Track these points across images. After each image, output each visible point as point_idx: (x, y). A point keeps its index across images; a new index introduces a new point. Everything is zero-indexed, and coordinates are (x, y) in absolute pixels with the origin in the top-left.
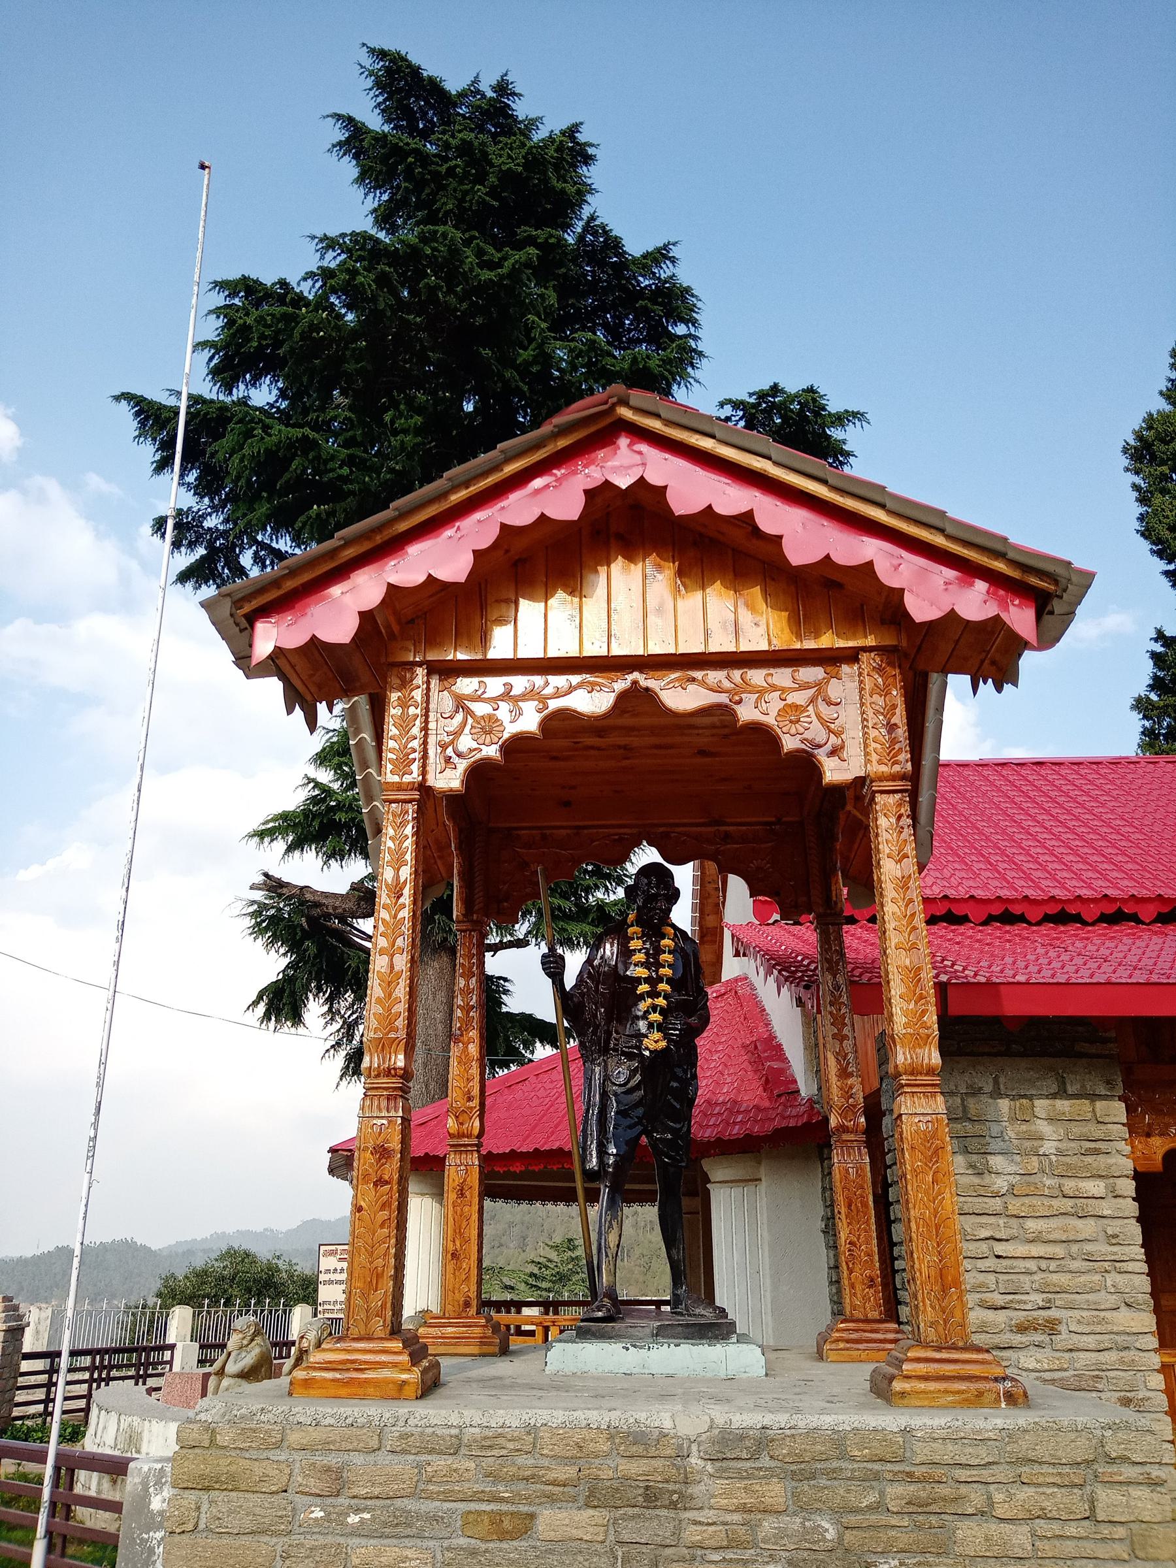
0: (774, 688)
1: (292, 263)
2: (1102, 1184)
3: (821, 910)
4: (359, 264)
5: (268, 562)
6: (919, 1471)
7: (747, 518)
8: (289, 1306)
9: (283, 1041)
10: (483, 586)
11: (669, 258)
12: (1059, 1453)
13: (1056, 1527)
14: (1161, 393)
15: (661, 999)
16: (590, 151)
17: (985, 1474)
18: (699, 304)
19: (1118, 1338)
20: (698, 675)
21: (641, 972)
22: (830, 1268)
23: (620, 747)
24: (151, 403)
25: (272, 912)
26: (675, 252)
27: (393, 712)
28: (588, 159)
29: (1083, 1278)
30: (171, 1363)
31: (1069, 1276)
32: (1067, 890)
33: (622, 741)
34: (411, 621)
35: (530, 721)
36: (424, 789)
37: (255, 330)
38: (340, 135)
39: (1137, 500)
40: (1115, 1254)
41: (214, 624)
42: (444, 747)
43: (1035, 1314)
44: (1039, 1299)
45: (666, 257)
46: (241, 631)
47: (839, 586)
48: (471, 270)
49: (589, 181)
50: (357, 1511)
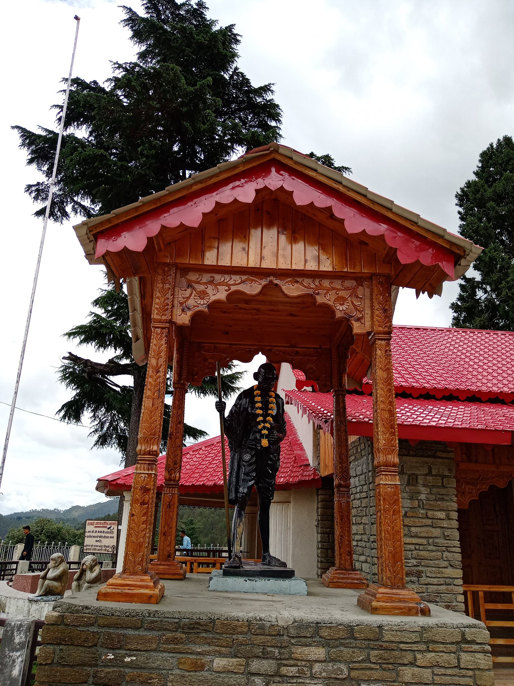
0: (333, 289)
1: (101, 73)
2: (444, 513)
3: (337, 388)
4: (131, 78)
5: (79, 211)
6: (384, 645)
7: (329, 209)
8: (70, 545)
9: (70, 428)
10: (203, 230)
11: (270, 90)
12: (446, 638)
13: (443, 671)
14: (474, 172)
15: (268, 424)
16: (239, 38)
17: (414, 647)
18: (282, 113)
19: (447, 580)
20: (300, 280)
21: (259, 412)
22: (318, 542)
23: (255, 309)
24: (29, 132)
25: (71, 370)
26: (273, 88)
27: (158, 285)
28: (237, 41)
29: (434, 553)
30: (16, 569)
31: (428, 552)
32: (408, 383)
33: (257, 307)
34: (170, 243)
35: (222, 295)
36: (171, 322)
37: (83, 101)
38: (126, 17)
39: (460, 218)
40: (448, 544)
41: (78, 237)
42: (181, 304)
43: (413, 568)
44: (414, 562)
45: (269, 90)
46: (90, 242)
47: (366, 244)
48: (183, 86)
49: (236, 51)
50: (130, 656)
